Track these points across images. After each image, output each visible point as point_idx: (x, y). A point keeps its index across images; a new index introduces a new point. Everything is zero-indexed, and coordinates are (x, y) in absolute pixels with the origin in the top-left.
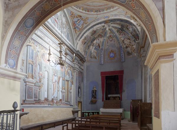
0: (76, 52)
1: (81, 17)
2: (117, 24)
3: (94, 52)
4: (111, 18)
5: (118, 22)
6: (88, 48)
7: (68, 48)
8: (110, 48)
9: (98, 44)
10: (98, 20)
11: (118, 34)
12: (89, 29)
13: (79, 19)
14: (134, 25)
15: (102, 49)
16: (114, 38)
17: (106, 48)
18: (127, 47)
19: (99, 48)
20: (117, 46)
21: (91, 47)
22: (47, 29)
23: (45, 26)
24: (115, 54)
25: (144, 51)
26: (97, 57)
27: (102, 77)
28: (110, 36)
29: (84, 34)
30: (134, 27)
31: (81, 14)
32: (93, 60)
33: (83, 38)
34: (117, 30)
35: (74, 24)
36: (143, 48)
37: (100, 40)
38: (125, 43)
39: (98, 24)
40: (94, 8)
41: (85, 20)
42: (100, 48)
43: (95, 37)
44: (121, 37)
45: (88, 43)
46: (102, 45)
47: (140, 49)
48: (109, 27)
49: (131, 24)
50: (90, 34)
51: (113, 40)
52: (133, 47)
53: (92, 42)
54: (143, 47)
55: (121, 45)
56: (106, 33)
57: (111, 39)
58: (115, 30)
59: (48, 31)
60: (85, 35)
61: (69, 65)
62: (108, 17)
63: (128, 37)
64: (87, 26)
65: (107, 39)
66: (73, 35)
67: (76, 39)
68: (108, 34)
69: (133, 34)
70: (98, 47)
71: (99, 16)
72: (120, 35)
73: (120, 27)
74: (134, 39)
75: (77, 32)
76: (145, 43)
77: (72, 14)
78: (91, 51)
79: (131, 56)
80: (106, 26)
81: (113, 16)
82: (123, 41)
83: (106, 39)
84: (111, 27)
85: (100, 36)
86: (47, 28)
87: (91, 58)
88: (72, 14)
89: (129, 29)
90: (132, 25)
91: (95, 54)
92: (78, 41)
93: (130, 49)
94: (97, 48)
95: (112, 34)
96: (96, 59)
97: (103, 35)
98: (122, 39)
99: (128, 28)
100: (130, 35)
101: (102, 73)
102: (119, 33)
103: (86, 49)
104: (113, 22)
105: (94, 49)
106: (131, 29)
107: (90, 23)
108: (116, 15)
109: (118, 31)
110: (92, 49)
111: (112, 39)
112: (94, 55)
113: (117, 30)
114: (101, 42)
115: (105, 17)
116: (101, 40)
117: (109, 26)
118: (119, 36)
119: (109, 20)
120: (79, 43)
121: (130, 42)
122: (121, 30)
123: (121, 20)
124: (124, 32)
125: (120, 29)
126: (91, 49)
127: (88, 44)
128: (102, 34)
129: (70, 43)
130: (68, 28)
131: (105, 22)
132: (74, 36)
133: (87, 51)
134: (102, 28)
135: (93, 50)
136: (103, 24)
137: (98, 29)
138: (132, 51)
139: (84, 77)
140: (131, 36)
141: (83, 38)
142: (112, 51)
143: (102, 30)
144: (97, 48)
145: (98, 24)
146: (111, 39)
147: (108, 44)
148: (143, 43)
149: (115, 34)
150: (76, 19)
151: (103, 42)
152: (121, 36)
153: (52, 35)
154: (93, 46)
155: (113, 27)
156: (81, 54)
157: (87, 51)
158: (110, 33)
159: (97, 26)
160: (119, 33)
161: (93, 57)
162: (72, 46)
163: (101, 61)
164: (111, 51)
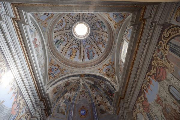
0: (45, 95)
1: (59, 66)
2: (91, 80)
4: (86, 73)
5: (92, 78)
6: (58, 100)
7: (37, 86)
8: (81, 103)
9: (69, 98)
10: (75, 72)
11: (91, 90)
12: (64, 79)
13: (56, 67)
14: (108, 81)
15: (72, 104)
17: (77, 104)
18: (99, 105)
19: (70, 102)
20: (89, 103)
21: (61, 99)
22: (23, 48)
23: (23, 43)
24: (87, 111)
25: (124, 103)
26: (65, 113)
28: (83, 91)
29: (58, 81)
30: (108, 82)
31: (60, 65)
32: (60, 115)
33: (55, 86)
35: (51, 70)
36: (123, 100)
37: (72, 93)
38: (97, 100)
39: (73, 76)
40: (72, 64)
41: (62, 71)
42: (71, 102)
43: (68, 89)
44: (94, 94)
45: (60, 92)
46: (74, 100)
47: (120, 101)
48: (83, 81)
49: (104, 80)
50: (63, 84)
51: (85, 95)
52: (106, 104)
53: (63, 94)
54: (123, 98)
55: (94, 101)
57: (83, 95)
58: (88, 86)
59: (24, 51)
60: (59, 83)
61: (29, 109)
62: (84, 72)
63: (100, 94)
64: (63, 76)
66: (46, 81)
67: (49, 84)
68: (81, 89)
69: (105, 91)
70: (68, 101)
71: (75, 70)
72: (93, 91)
73: (93, 83)
74: (107, 95)
75: (51, 78)
76: (125, 93)
78: (60, 104)
79: (106, 114)
80: (81, 80)
81: (88, 72)
82: (95, 97)
84: (84, 82)
85: (73, 89)
86: (24, 47)
87: (59, 112)
88: (52, 62)
89: (102, 86)
90: (105, 81)
92: (49, 86)
93: (103, 106)
94: (67, 101)
95: (84, 90)
96: (64, 114)
97: (76, 89)
98: (95, 95)
99: (101, 85)
100: (103, 92)
103: (55, 100)
104: (88, 77)
105: (64, 102)
106: (103, 86)
107: (66, 74)
108: (90, 72)
109: (91, 87)
110: (62, 102)
111: (84, 94)
112: (62, 109)
114: (72, 95)
115: (82, 72)
116: (73, 93)
117: (83, 81)
118: (92, 93)
119: (84, 74)
120: (49, 89)
121: (103, 99)
122: (94, 87)
123: (95, 76)
124: (96, 88)
125: (93, 85)
126: (60, 101)
127: (58, 94)
128: (75, 88)
129: (42, 78)
130: (44, 71)
131: (81, 76)
132: (47, 80)
133: (56, 103)
134: (77, 81)
135: (62, 103)
136: (78, 78)
137: (73, 81)
138: (106, 109)
140: (104, 93)
141: (55, 86)
142: (83, 108)
143: (77, 83)
144: (67, 101)
145: (73, 76)
146: (83, 95)
147: (80, 100)
148: (123, 93)
150: (53, 67)
151: (75, 96)
153: (26, 58)
155: (86, 82)
156: (49, 101)
157: (56, 103)
158: (83, 88)
159: (73, 78)
161: (60, 111)
162: (43, 82)
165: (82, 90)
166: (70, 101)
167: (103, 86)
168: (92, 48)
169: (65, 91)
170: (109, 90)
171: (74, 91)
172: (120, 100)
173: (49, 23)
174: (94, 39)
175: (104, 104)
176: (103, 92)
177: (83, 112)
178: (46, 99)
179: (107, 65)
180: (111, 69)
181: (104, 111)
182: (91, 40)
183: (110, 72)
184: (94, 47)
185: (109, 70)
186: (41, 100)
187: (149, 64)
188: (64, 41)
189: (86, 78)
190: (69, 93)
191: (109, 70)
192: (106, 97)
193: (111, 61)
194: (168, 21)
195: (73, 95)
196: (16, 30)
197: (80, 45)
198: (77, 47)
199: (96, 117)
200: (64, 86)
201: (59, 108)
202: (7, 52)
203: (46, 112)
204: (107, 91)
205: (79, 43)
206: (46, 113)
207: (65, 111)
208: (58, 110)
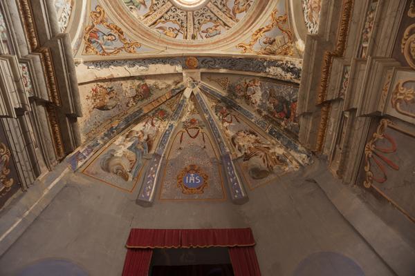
3: (124, 155)
8: (185, 157)
9: (145, 137)
11: (217, 118)
15: (157, 156)
16: (205, 128)
18: (247, 157)
19: (150, 149)
20: (212, 155)
21: (120, 138)
27: (133, 253)
28: (192, 122)
34: (214, 104)
37: (157, 125)
38: (239, 146)
42: (152, 152)
44: (227, 129)
48: (194, 87)
51: (200, 133)
54: (340, 55)
55: (228, 151)
56: (180, 106)
58: (209, 104)
63: (248, 128)
65: (181, 129)
69: (264, 113)
72: (223, 121)
73: (224, 94)
77: (100, 13)
82: (233, 139)
83: (177, 127)
84: (197, 90)
88: (100, 13)
89: (253, 99)
91: (126, 165)
94: (140, 147)
95: (197, 117)
96: (127, 179)
98: (231, 133)
101: (135, 235)
102: (219, 114)
105: (129, 149)
106: (257, 97)
109: (217, 109)
111: (196, 131)
113: (214, 104)
114: (158, 131)
116: (162, 126)
118: (220, 126)
119: (197, 57)
126: (117, 143)
127: (111, 119)
131: (187, 62)
133: (101, 142)
135: (124, 149)
138: (271, 163)
139: (16, 208)
142: (193, 169)
144: (140, 147)
149: (207, 116)
151: (165, 135)
152: (226, 124)
154: (127, 137)
155: (203, 89)
157: (101, 142)
158: (192, 112)
160: (219, 114)
163: (143, 190)
164: (188, 168)
165: (191, 118)
166: (150, 147)
167: (257, 97)
168: (218, 28)
169: (134, 114)
170: (276, 102)
171: (163, 119)
172: (329, 63)
173: (111, 17)
174: (224, 6)
175: (263, 154)
176: (258, 116)
177: (192, 179)
178: (54, 54)
179: (266, 29)
180: (278, 38)
181: (264, 171)
182: (215, 10)
183: (275, 47)
184: (225, 25)
185: (272, 43)
186: (34, 50)
187: (395, 28)
188: (142, 7)
189: (202, 73)
190: (146, 123)
191: (274, 40)
192: (267, 131)
193: (277, 16)
194: (381, 110)
195: (162, 130)
196: (50, 92)
197: (185, 25)
198: (178, 28)
199: (238, 189)
200: (134, 98)
201: (109, 159)
202: (16, 134)
203: (57, 128)
204: (269, 110)
205: (183, 18)
206: (54, 130)
207: (130, 172)
208: (108, 164)
